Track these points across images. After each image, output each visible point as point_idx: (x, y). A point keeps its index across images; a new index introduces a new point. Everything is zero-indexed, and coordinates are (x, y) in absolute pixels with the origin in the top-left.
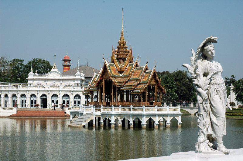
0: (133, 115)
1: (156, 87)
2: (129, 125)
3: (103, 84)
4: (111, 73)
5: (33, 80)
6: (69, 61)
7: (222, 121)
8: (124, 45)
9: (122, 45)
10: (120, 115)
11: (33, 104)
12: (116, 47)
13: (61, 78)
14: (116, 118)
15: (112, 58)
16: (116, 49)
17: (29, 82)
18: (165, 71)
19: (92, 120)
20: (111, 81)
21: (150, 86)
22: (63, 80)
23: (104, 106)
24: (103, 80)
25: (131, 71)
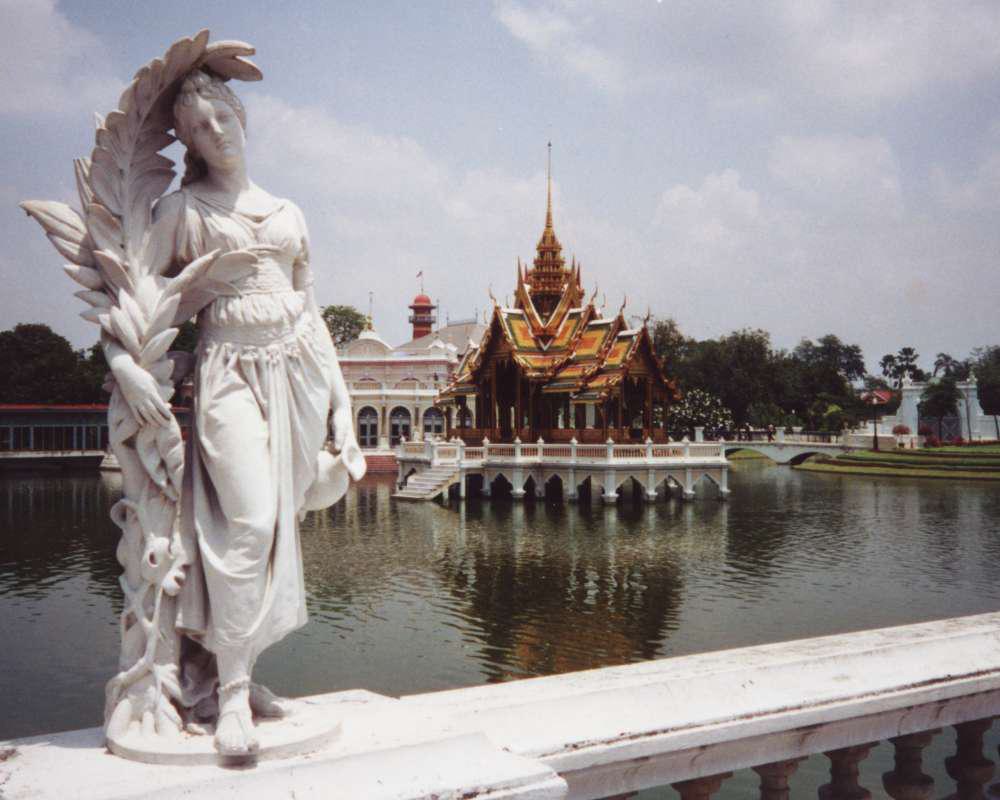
2: (320, 520)
3: (489, 374)
4: (516, 340)
7: (246, 550)
9: (549, 250)
10: (539, 468)
12: (529, 259)
16: (531, 267)
18: (784, 342)
19: (458, 485)
21: (631, 379)
23: (493, 440)
24: (492, 364)
25: (573, 332)
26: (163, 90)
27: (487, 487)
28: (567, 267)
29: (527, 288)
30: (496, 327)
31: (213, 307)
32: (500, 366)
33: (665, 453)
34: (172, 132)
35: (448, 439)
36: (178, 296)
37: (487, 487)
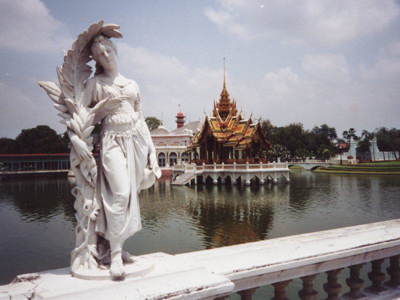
1: (261, 142)
3: (204, 140)
9: (225, 96)
10: (222, 173)
12: (218, 99)
14: (265, 177)
16: (219, 102)
20: (213, 137)
23: (206, 164)
28: (231, 102)
29: (217, 109)
30: (207, 123)
32: (208, 137)
33: (267, 167)
34: (91, 57)
35: (190, 163)
36: (94, 114)
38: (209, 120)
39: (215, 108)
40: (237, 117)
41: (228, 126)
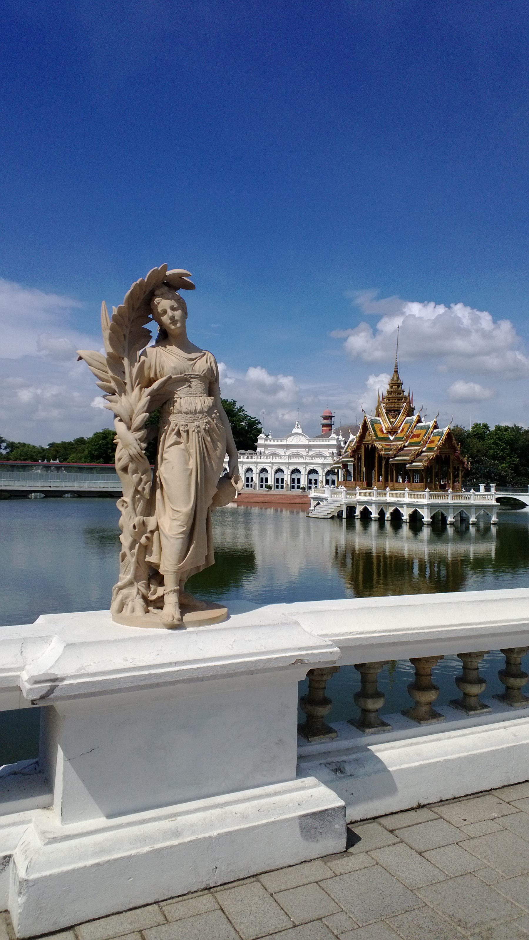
0: (409, 505)
3: (362, 452)
5: (266, 446)
6: (331, 417)
8: (398, 387)
11: (294, 483)
13: (307, 443)
15: (377, 409)
16: (385, 394)
17: (259, 449)
22: (310, 447)
23: (361, 488)
24: (363, 446)
26: (146, 294)
27: (358, 513)
28: (406, 394)
31: (167, 404)
34: (150, 316)
35: (337, 487)
36: (149, 397)
37: (358, 513)
38: (369, 420)
39: (379, 404)
40: (415, 418)
41: (399, 431)
